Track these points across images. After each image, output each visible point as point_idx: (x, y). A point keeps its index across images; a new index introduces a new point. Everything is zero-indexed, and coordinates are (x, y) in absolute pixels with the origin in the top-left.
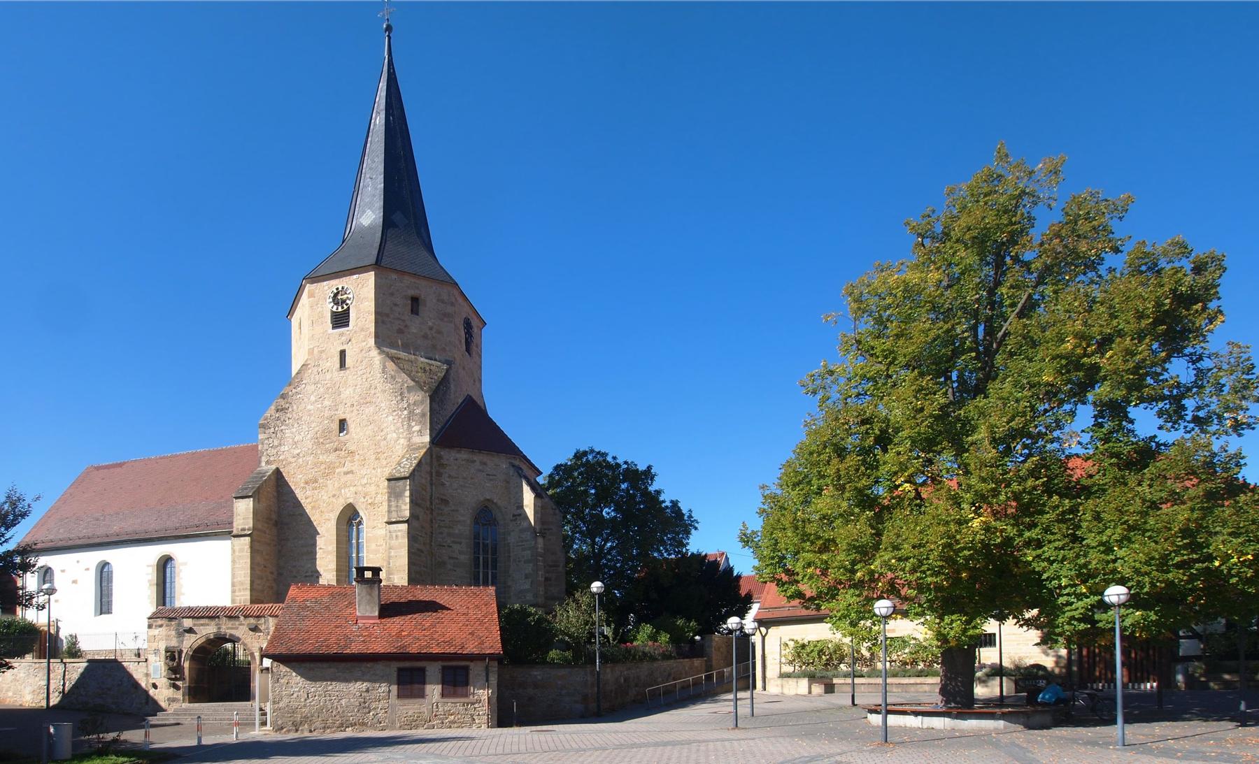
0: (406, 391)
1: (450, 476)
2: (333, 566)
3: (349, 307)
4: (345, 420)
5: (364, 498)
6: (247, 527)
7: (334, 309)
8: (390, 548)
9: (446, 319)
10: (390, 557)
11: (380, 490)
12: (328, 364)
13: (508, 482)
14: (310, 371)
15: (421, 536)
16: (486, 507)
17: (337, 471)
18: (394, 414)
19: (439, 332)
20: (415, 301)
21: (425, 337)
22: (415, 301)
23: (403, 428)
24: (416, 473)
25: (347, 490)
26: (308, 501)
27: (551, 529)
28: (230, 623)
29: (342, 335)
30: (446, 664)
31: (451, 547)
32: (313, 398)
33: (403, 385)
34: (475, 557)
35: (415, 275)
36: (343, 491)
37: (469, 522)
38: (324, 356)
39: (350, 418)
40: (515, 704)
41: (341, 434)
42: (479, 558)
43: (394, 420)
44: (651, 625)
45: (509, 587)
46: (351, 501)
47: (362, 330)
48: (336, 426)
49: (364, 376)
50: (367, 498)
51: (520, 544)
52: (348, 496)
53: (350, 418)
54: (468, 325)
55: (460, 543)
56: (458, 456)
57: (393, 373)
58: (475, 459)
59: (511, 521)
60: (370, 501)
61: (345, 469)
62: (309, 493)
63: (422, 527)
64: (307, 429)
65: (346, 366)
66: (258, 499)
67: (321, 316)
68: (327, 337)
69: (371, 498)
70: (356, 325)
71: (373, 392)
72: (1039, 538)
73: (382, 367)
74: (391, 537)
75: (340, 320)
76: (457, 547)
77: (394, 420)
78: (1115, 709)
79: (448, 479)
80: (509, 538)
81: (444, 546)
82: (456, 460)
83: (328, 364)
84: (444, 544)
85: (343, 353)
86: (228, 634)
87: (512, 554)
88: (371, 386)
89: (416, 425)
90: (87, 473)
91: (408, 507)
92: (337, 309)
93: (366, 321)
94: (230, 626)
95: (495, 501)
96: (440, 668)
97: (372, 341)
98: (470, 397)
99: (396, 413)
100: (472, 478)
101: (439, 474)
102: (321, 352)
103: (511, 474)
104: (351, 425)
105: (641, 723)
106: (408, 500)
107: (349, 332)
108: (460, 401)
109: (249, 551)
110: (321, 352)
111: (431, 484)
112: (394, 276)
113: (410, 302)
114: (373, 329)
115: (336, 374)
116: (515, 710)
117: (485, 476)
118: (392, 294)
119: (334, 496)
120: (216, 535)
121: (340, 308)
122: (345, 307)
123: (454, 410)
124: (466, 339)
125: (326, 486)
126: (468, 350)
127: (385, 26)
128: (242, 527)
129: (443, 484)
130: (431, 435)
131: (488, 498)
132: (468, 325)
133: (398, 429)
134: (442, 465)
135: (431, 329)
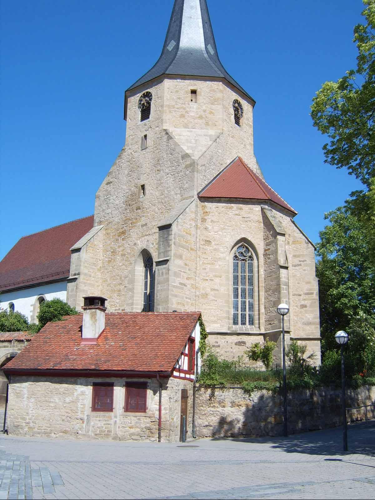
1: (212, 221)
15: (184, 272)
21: (201, 117)
27: (306, 261)
30: (130, 380)
44: (334, 338)
46: (145, 247)
76: (217, 280)
78: (281, 348)
81: (207, 280)
84: (207, 278)
98: (239, 158)
105: (207, 489)
108: (229, 162)
117: (241, 219)
118: (177, 91)
124: (236, 115)
128: (75, 272)
135: (205, 111)
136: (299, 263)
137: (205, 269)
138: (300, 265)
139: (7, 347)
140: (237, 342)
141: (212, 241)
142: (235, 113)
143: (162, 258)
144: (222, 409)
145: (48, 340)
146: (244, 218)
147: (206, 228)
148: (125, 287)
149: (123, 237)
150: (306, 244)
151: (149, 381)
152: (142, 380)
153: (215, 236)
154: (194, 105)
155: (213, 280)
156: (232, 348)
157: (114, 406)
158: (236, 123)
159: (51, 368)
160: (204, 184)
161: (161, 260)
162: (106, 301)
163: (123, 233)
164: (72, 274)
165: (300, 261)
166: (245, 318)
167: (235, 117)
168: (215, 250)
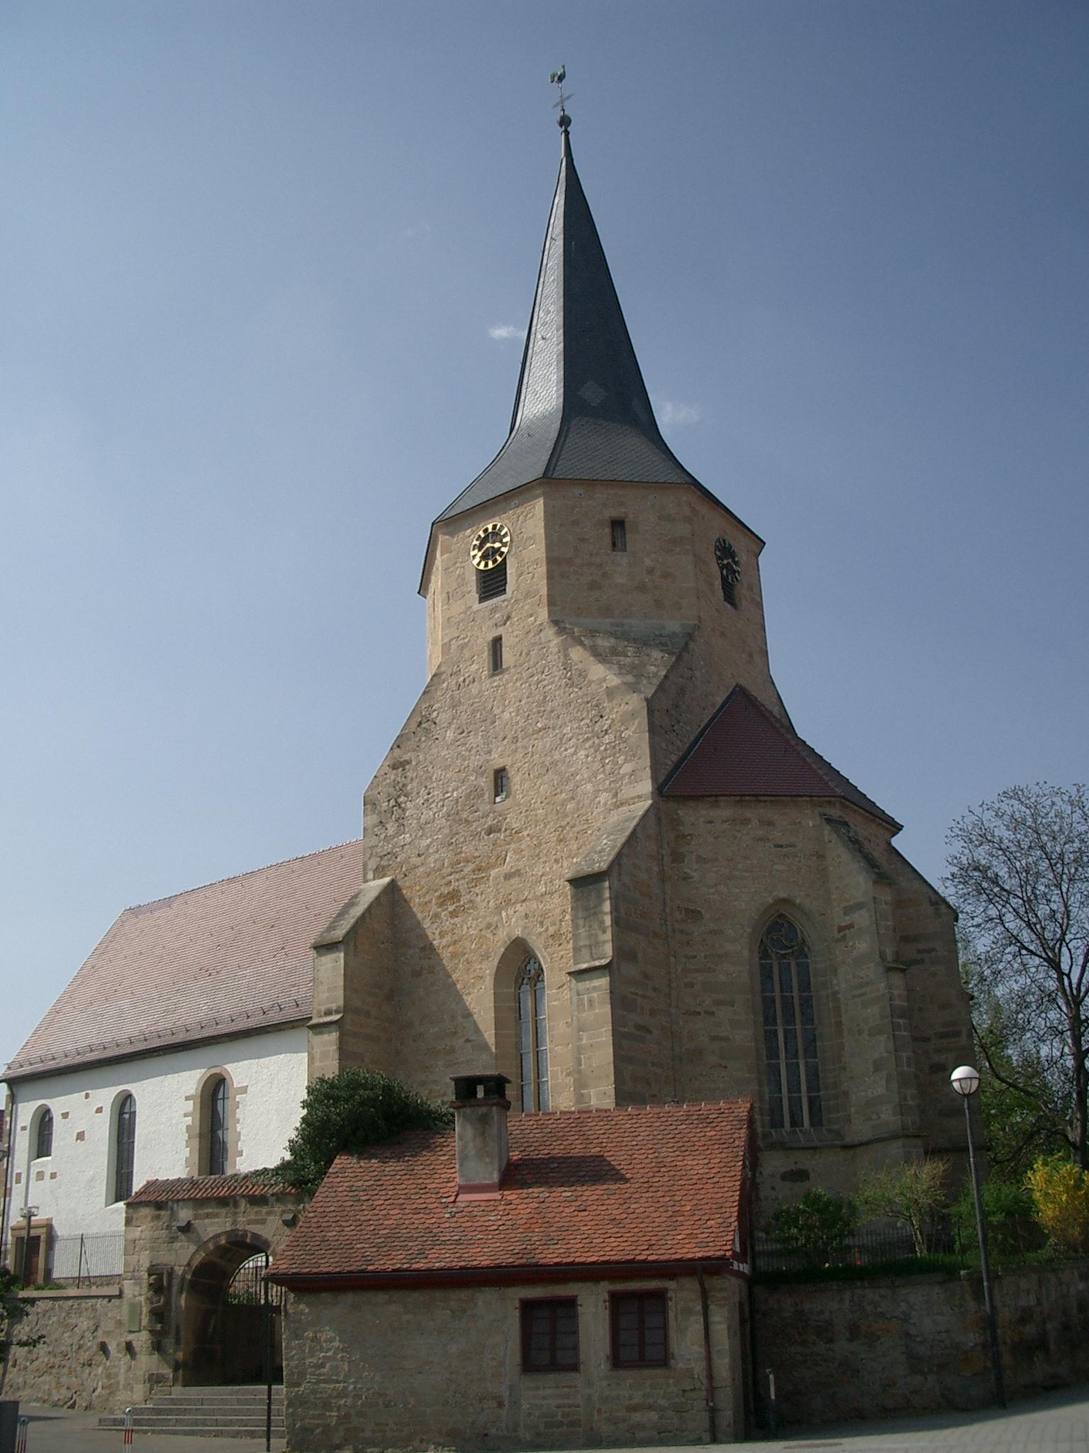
1: (700, 859)
3: (505, 559)
4: (503, 769)
5: (542, 923)
6: (334, 1006)
7: (482, 567)
8: (580, 1030)
9: (678, 549)
10: (580, 1050)
11: (561, 902)
12: (475, 667)
13: (821, 857)
15: (645, 997)
16: (781, 916)
17: (493, 872)
18: (587, 745)
19: (666, 575)
20: (618, 525)
21: (642, 588)
22: (618, 525)
23: (603, 772)
24: (625, 860)
25: (510, 912)
26: (444, 941)
27: (933, 950)
28: (253, 1212)
29: (494, 610)
30: (620, 1287)
31: (713, 1013)
32: (450, 735)
34: (766, 1031)
35: (613, 483)
36: (504, 914)
37: (746, 954)
39: (512, 766)
40: (771, 1377)
41: (498, 799)
42: (775, 1033)
43: (587, 756)
45: (846, 1094)
46: (518, 932)
47: (528, 595)
48: (486, 783)
50: (547, 923)
51: (857, 992)
52: (513, 925)
53: (512, 766)
54: (725, 551)
55: (732, 1004)
56: (714, 813)
58: (749, 815)
59: (837, 941)
60: (552, 930)
61: (506, 868)
62: (447, 925)
63: (646, 976)
64: (441, 797)
66: (356, 947)
67: (462, 580)
69: (553, 924)
70: (518, 589)
74: (580, 1004)
75: (492, 583)
77: (587, 756)
79: (696, 866)
80: (835, 982)
82: (711, 822)
83: (475, 667)
85: (497, 643)
87: (844, 1019)
88: (546, 697)
89: (626, 761)
90: (121, 922)
91: (608, 936)
92: (486, 565)
93: (533, 577)
95: (798, 901)
96: (606, 1296)
97: (543, 614)
98: (740, 687)
99: (591, 742)
100: (746, 858)
101: (678, 858)
102: (462, 647)
103: (826, 838)
104: (516, 781)
106: (608, 920)
107: (506, 603)
109: (337, 1056)
110: (462, 647)
111: (663, 881)
112: (577, 491)
113: (607, 530)
114: (544, 591)
115: (487, 683)
116: (773, 1397)
118: (575, 523)
119: (489, 926)
120: (293, 1028)
121: (490, 563)
122: (499, 559)
123: (706, 721)
124: (724, 579)
125: (474, 908)
126: (730, 597)
129: (686, 878)
130: (654, 778)
131: (782, 895)
132: (725, 551)
133: (595, 774)
134: (681, 837)
135: (650, 571)
136: (919, 957)
137: (691, 985)
138: (922, 961)
139: (217, 1215)
140: (786, 1172)
141: (703, 912)
142: (722, 573)
143: (585, 962)
144: (827, 1345)
145: (362, 1193)
146: (781, 846)
147: (685, 879)
148: (468, 1041)
149: (451, 908)
150: (932, 905)
151: (671, 1285)
152: (652, 1284)
153: (711, 896)
154: (622, 559)
155: (713, 1013)
156: (773, 1188)
157: (582, 1357)
158: (725, 600)
159: (405, 1266)
160: (670, 763)
161: (584, 966)
162: (507, 1085)
163: (454, 896)
164: (319, 1011)
165: (919, 952)
166: (801, 1107)
167: (723, 585)
168: (713, 932)
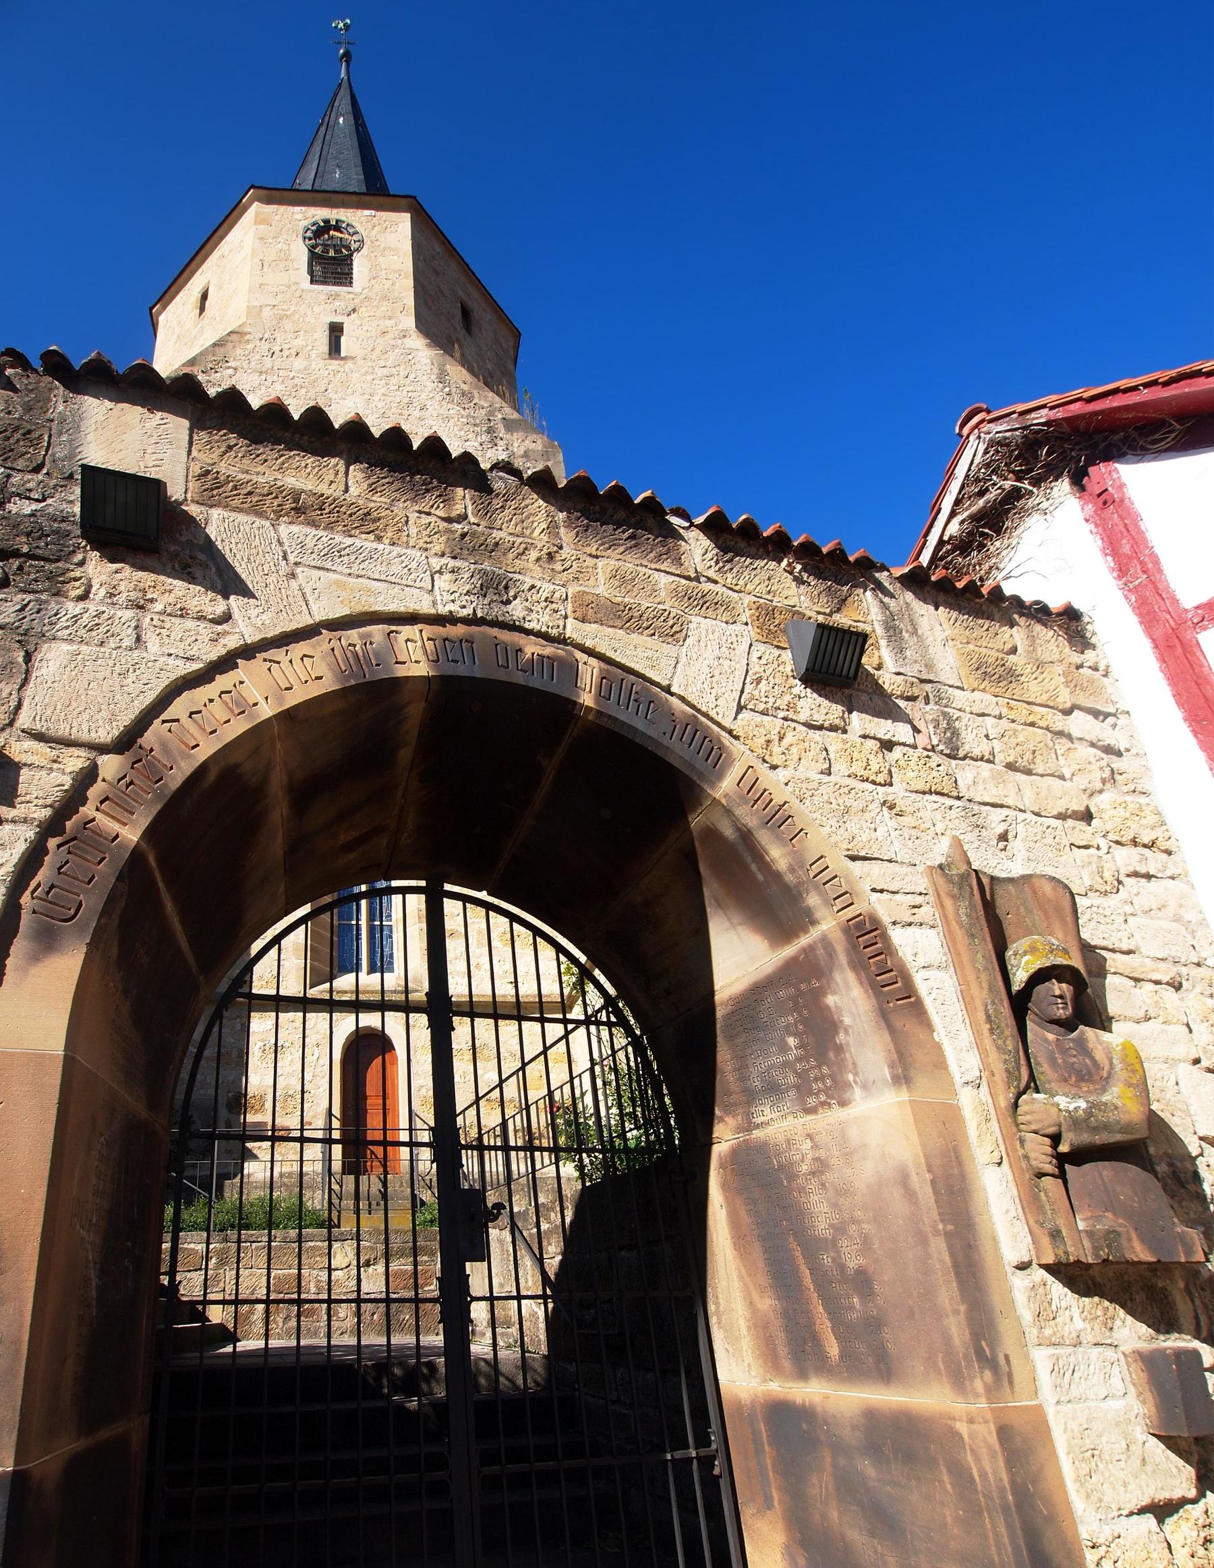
0: (501, 427)
2: (211, 1038)
14: (250, 346)
33: (491, 413)
38: (288, 325)
49: (393, 381)
57: (465, 387)
65: (343, 354)
68: (297, 294)
71: (417, 414)
72: (710, 1446)
73: (436, 371)
86: (590, 671)
94: (602, 588)
107: (352, 296)
127: (342, 51)
